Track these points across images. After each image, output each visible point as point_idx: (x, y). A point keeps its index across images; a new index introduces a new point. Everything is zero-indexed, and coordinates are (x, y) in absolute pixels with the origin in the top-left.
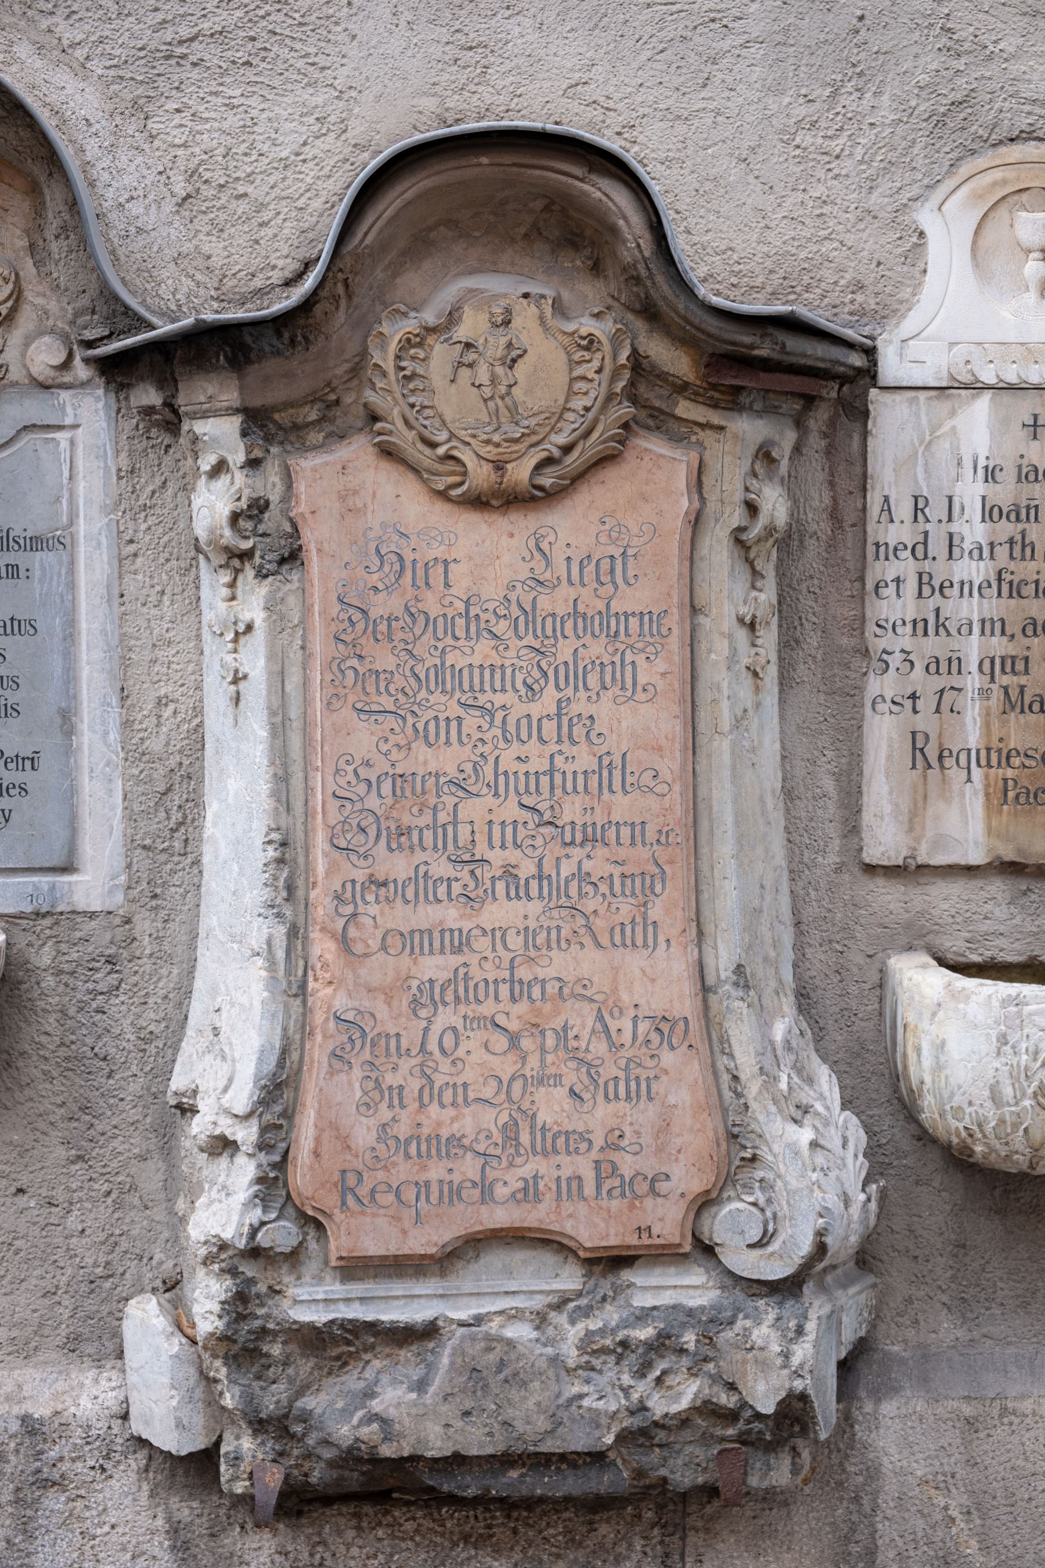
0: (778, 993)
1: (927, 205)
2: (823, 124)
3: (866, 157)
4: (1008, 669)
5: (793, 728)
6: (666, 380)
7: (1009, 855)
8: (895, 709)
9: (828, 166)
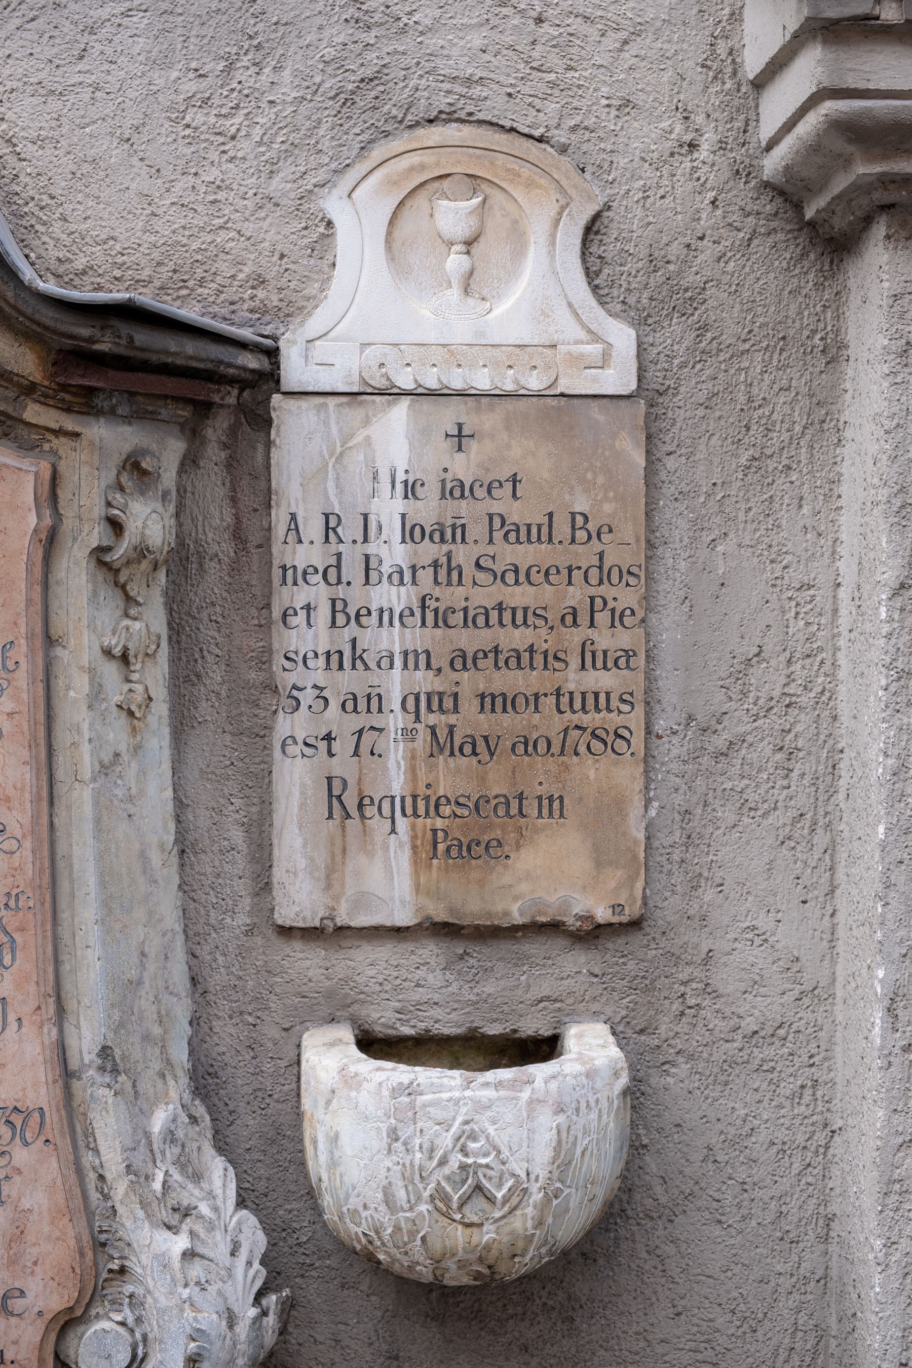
0: (163, 1076)
1: (335, 191)
2: (216, 101)
3: (265, 138)
4: (435, 707)
5: (196, 773)
6: (10, 381)
7: (441, 916)
8: (308, 751)
9: (222, 148)
